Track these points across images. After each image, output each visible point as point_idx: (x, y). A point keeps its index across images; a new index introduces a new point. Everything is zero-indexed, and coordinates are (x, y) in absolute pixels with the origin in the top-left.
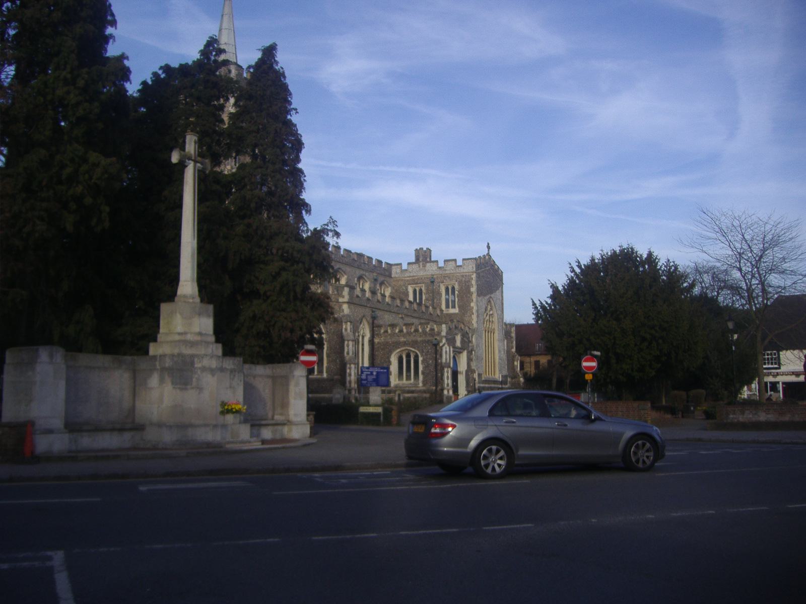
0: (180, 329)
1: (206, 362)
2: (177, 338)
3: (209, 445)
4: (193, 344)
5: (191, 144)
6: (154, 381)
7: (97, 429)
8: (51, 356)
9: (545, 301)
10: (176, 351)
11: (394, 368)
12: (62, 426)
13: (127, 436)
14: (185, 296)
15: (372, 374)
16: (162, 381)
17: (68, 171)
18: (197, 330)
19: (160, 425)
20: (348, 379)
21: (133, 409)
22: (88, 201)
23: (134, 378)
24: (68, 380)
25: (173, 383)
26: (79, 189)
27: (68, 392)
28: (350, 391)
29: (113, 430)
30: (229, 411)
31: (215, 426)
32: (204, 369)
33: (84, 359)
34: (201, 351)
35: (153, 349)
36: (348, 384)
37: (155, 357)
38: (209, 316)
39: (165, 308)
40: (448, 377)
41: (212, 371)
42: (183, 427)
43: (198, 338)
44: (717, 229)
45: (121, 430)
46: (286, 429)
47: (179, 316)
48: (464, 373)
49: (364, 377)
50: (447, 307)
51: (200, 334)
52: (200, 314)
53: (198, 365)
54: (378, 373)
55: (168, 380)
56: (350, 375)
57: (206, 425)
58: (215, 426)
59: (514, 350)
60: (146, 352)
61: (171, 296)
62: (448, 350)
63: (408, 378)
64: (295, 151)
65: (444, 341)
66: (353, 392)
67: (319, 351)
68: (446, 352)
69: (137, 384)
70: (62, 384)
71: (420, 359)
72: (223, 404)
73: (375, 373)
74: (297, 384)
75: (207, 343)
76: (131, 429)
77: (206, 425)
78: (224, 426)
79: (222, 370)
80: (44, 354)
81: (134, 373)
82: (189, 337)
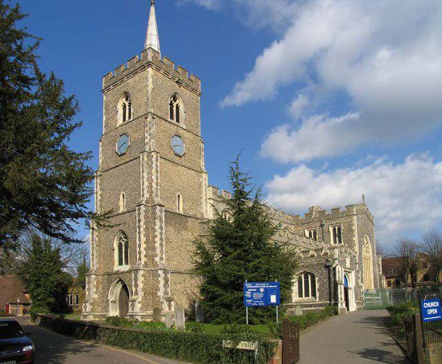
11: (295, 288)
40: (341, 292)
48: (353, 288)
50: (335, 242)
59: (381, 272)
62: (340, 269)
63: (307, 295)
65: (337, 262)
68: (339, 271)
71: (317, 279)
73: (262, 290)
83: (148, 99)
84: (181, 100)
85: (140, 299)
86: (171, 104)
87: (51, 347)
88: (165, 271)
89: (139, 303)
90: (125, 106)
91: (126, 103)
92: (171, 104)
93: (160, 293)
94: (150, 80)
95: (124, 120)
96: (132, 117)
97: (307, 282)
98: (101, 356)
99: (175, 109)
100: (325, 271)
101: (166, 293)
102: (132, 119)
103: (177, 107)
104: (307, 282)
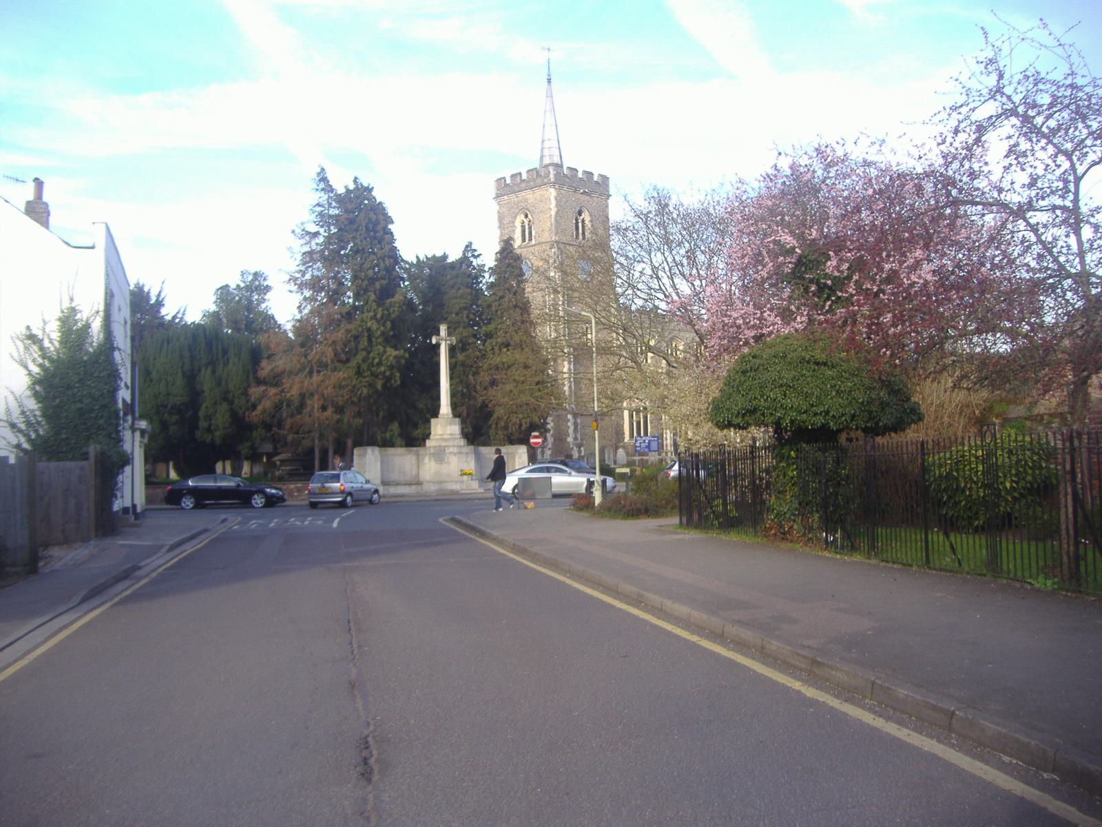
0: (440, 432)
1: (451, 449)
2: (439, 437)
3: (452, 491)
4: (446, 440)
5: (443, 329)
6: (427, 460)
7: (398, 484)
8: (373, 451)
9: (119, 306)
10: (438, 444)
12: (380, 482)
13: (414, 487)
14: (443, 415)
15: (644, 441)
16: (430, 459)
17: (377, 360)
18: (449, 432)
19: (429, 482)
20: (665, 443)
21: (418, 475)
22: (388, 373)
23: (418, 459)
24: (382, 463)
25: (435, 461)
26: (383, 369)
27: (381, 467)
28: (666, 453)
29: (406, 484)
30: (465, 474)
31: (457, 482)
32: (450, 453)
33: (391, 451)
34: (451, 443)
35: (428, 443)
36: (665, 448)
37: (430, 447)
38: (456, 424)
39: (433, 421)
41: (455, 454)
42: (441, 482)
43: (450, 437)
44: (1038, 45)
45: (410, 485)
46: (444, 484)
47: (439, 426)
49: (638, 444)
51: (451, 434)
52: (450, 424)
53: (447, 451)
54: (650, 441)
55: (432, 458)
56: (666, 439)
57: (452, 482)
58: (457, 482)
60: (425, 445)
61: (435, 413)
64: (561, 314)
66: (669, 454)
67: (543, 435)
69: (419, 464)
70: (379, 464)
72: (462, 471)
74: (520, 457)
75: (456, 439)
76: (415, 484)
77: (452, 482)
78: (462, 482)
79: (460, 453)
80: (369, 450)
81: (418, 456)
82: (445, 436)
83: (551, 225)
84: (587, 213)
85: (550, 446)
86: (577, 220)
87: (108, 811)
88: (575, 416)
89: (549, 449)
90: (523, 227)
91: (525, 220)
92: (577, 220)
93: (570, 439)
94: (553, 202)
95: (524, 240)
96: (533, 240)
97: (639, 429)
98: (366, 775)
99: (580, 225)
100: (91, 245)
101: (576, 439)
102: (533, 242)
103: (583, 221)
104: (639, 429)
